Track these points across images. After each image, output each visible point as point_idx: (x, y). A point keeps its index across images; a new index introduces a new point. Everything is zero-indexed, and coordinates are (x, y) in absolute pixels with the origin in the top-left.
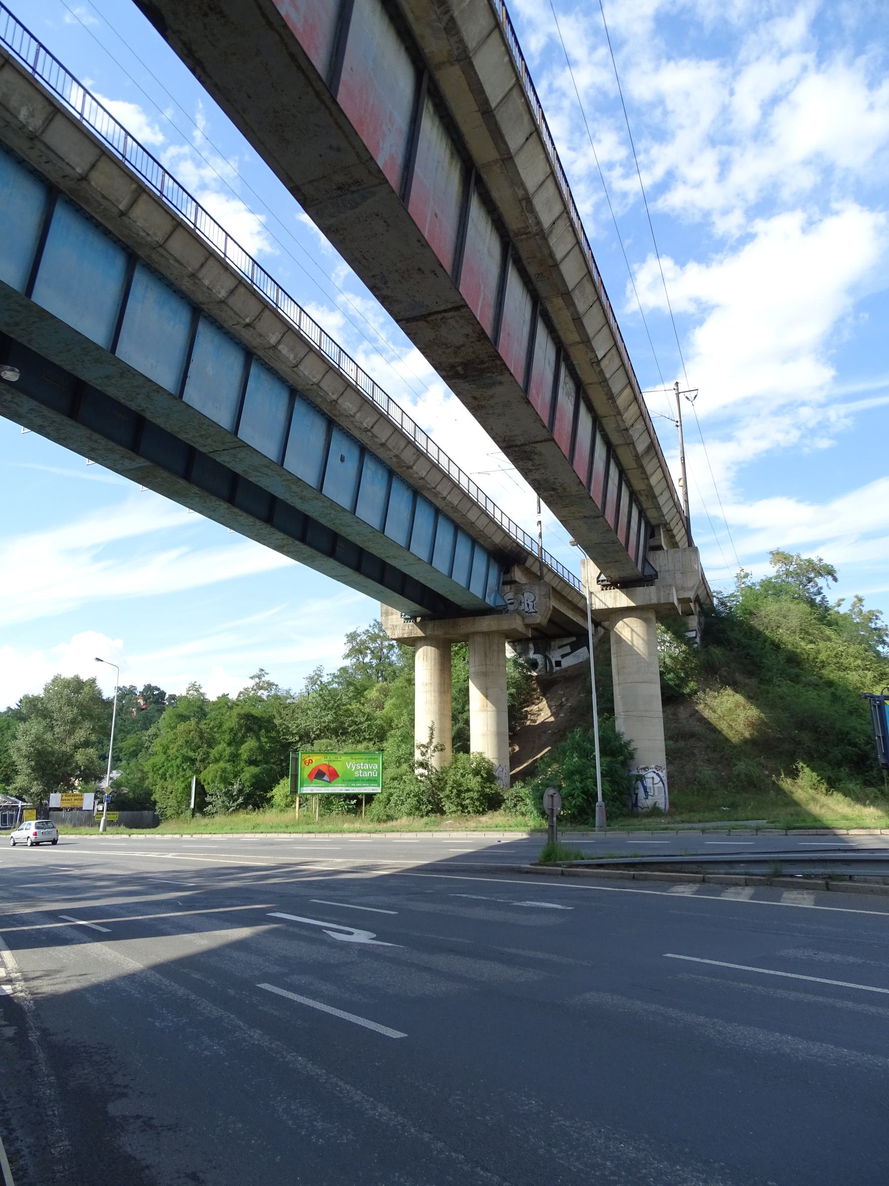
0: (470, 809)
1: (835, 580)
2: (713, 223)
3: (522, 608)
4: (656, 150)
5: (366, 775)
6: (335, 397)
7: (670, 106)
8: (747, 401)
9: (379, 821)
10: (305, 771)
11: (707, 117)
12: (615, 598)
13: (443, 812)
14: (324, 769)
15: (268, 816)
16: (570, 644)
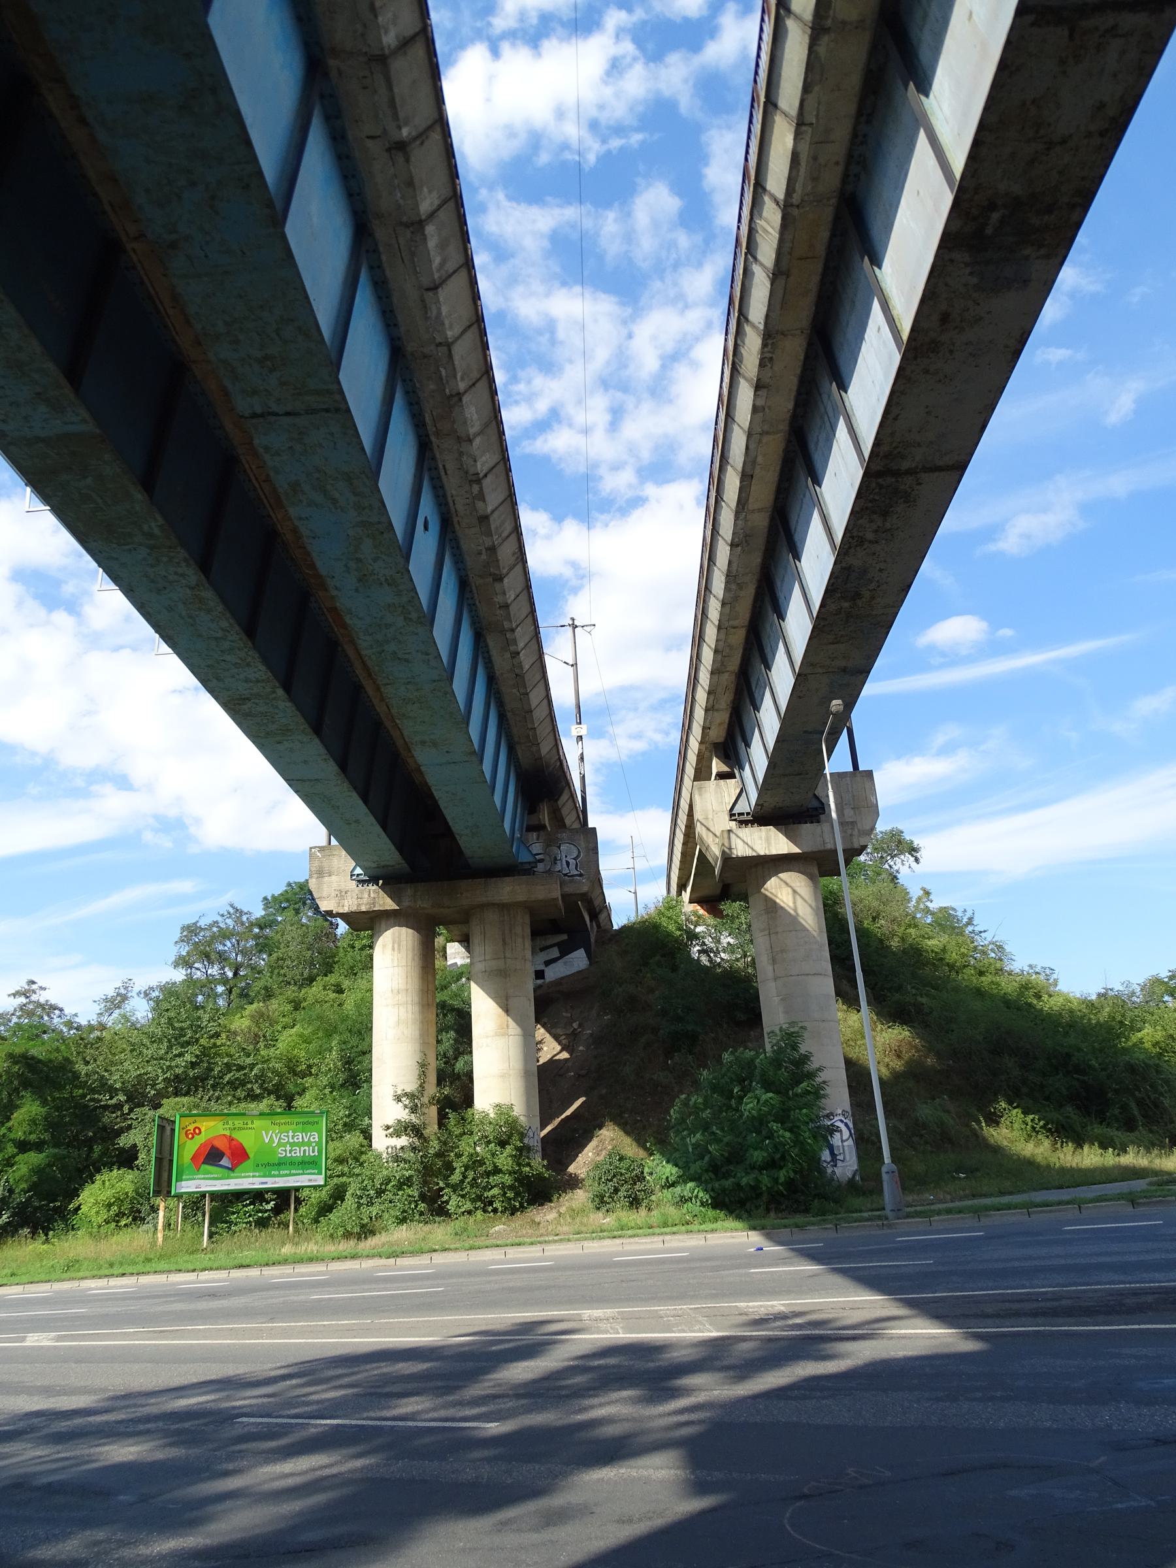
0: (497, 1205)
1: (917, 860)
2: (601, 477)
3: (558, 868)
4: (539, 381)
5: (298, 1153)
6: (462, 386)
7: (561, 335)
8: (624, 689)
9: (348, 1235)
10: (186, 1149)
11: (602, 355)
12: (768, 840)
13: (447, 1214)
14: (221, 1145)
15: (72, 1245)
16: (558, 945)
